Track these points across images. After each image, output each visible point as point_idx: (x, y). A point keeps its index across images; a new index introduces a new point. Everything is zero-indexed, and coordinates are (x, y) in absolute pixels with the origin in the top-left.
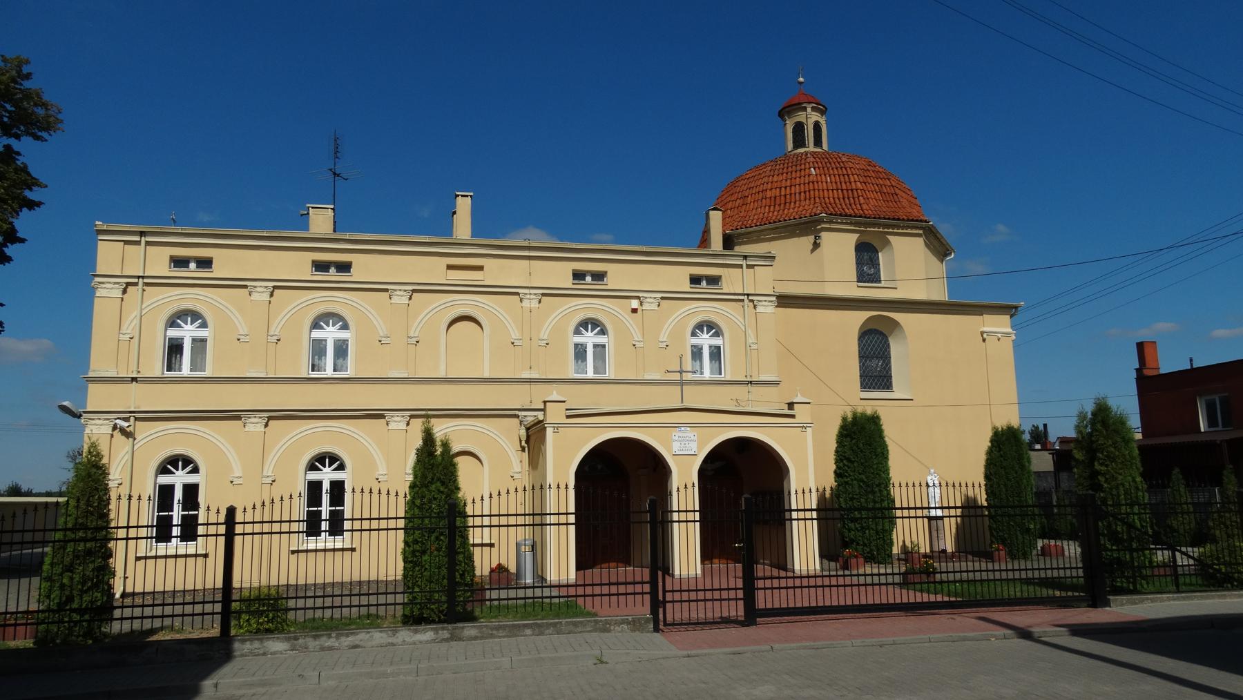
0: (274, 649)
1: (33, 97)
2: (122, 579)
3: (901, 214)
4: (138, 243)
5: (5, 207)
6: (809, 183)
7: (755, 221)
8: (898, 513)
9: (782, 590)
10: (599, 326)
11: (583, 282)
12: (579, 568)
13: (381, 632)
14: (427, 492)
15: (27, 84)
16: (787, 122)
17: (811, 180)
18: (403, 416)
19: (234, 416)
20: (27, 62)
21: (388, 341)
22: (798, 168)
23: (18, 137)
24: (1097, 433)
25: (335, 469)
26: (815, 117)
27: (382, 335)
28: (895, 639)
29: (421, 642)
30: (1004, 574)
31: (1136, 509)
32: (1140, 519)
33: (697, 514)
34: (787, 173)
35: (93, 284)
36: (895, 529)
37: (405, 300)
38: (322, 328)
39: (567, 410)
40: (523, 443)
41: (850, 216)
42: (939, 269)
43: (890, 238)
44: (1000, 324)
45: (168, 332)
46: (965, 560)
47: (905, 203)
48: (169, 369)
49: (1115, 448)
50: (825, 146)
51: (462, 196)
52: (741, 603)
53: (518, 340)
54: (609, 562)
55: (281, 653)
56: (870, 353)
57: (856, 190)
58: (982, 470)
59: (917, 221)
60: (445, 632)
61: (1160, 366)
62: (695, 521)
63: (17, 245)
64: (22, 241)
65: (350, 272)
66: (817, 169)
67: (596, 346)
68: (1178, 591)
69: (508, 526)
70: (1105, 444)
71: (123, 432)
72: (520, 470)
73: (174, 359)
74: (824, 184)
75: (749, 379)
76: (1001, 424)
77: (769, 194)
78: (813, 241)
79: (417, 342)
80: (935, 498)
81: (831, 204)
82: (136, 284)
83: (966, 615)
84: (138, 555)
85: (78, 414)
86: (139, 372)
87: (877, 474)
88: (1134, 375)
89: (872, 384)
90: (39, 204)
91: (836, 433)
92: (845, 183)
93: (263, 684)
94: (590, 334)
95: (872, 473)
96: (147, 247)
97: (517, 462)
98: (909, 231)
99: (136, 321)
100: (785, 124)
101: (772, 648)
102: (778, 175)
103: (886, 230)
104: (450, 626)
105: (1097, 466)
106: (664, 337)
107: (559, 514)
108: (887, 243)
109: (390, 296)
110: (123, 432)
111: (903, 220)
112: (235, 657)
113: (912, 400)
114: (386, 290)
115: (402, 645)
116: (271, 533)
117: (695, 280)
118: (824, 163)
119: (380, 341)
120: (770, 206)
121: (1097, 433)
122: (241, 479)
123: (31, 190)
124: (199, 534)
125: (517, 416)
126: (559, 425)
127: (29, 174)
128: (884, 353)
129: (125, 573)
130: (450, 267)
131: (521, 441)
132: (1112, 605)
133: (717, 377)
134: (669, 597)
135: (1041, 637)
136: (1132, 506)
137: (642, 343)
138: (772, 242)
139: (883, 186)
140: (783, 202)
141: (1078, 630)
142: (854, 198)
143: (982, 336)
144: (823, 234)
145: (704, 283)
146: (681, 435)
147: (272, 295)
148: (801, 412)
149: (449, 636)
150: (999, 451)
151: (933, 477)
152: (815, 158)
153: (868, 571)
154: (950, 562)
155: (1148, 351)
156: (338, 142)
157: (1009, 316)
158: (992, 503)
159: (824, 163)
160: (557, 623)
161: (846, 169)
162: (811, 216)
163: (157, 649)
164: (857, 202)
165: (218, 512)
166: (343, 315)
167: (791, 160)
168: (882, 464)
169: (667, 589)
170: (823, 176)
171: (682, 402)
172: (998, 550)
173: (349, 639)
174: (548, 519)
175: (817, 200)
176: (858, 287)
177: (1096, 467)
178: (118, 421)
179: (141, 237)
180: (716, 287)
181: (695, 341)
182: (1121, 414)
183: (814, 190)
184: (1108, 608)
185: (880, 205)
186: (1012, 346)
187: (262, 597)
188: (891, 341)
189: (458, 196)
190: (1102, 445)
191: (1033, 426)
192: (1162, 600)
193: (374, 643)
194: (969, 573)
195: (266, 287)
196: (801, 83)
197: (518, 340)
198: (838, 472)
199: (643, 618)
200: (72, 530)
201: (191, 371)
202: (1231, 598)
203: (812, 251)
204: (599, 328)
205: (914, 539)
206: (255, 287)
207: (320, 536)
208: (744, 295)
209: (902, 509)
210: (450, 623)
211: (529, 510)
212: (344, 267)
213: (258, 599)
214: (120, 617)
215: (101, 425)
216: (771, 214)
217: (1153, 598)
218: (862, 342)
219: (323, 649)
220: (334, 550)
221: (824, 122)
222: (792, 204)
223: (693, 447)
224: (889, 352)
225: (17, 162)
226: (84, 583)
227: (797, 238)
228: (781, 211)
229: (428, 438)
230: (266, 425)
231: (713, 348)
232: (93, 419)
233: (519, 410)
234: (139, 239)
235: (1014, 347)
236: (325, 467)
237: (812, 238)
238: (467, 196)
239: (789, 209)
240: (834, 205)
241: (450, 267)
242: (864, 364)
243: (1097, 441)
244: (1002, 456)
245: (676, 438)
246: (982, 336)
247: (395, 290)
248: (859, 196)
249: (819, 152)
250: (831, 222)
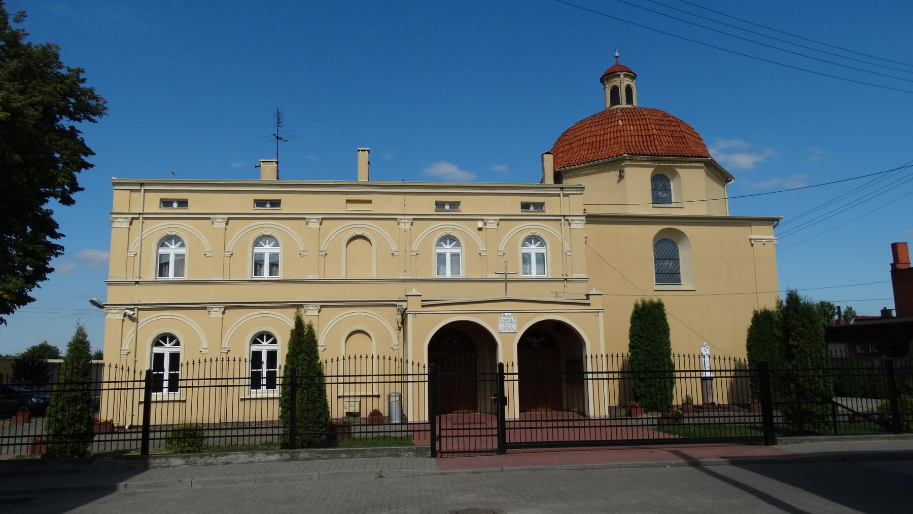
0: (174, 464)
1: (90, 93)
3: (687, 153)
4: (139, 191)
6: (617, 132)
7: (577, 161)
8: (677, 375)
9: (634, 427)
10: (539, 241)
12: (521, 411)
13: (244, 454)
14: (296, 360)
17: (618, 129)
18: (220, 308)
20: (83, 71)
21: (306, 254)
22: (610, 120)
23: (79, 120)
25: (271, 343)
26: (627, 81)
27: (301, 250)
29: (271, 461)
30: (747, 419)
34: (602, 125)
37: (317, 225)
38: (261, 246)
39: (422, 301)
40: (400, 325)
41: (647, 155)
43: (678, 170)
45: (255, 249)
47: (692, 144)
49: (804, 327)
50: (635, 103)
51: (362, 150)
53: (396, 251)
54: (463, 409)
57: (653, 135)
58: (745, 343)
59: (699, 157)
60: (287, 454)
61: (910, 261)
62: (425, 381)
63: (78, 193)
64: (82, 189)
66: (623, 121)
67: (452, 255)
68: (836, 434)
70: (796, 325)
71: (130, 317)
72: (398, 344)
73: (164, 268)
74: (629, 132)
75: (565, 277)
76: (760, 308)
78: (619, 174)
82: (138, 218)
83: (666, 449)
84: (339, 395)
85: (102, 306)
86: (140, 277)
87: (660, 346)
88: (890, 269)
90: (92, 166)
92: (645, 130)
95: (656, 346)
97: (395, 336)
98: (693, 165)
99: (139, 244)
100: (605, 88)
102: (595, 127)
103: (675, 164)
104: (290, 451)
105: (791, 342)
106: (502, 248)
107: (378, 375)
108: (676, 174)
109: (398, 223)
110: (130, 317)
111: (688, 156)
113: (695, 291)
115: (258, 463)
116: (228, 386)
117: (525, 206)
119: (300, 254)
120: (588, 150)
122: (207, 350)
130: (348, 201)
131: (398, 323)
132: (778, 443)
133: (542, 276)
134: (443, 433)
136: (816, 370)
138: (590, 176)
139: (674, 132)
141: (735, 462)
142: (651, 142)
143: (751, 242)
144: (627, 170)
145: (532, 208)
146: (505, 318)
148: (595, 303)
149: (290, 457)
150: (757, 329)
151: (705, 348)
153: (645, 416)
154: (716, 412)
155: (900, 249)
156: (280, 115)
160: (364, 450)
161: (645, 120)
162: (617, 156)
163: (100, 462)
164: (653, 144)
165: (141, 373)
167: (605, 115)
170: (628, 126)
171: (506, 295)
173: (223, 458)
174: (410, 378)
175: (623, 144)
176: (653, 207)
182: (808, 302)
183: (621, 136)
185: (671, 145)
189: (359, 150)
191: (848, 307)
192: (819, 441)
193: (240, 461)
194: (720, 418)
195: (223, 218)
196: (617, 57)
197: (396, 251)
202: (876, 440)
203: (619, 182)
204: (455, 242)
206: (216, 218)
207: (177, 391)
209: (680, 371)
210: (291, 449)
211: (249, 376)
212: (276, 204)
213: (184, 430)
218: (657, 248)
219: (206, 464)
220: (268, 399)
222: (605, 147)
223: (514, 327)
225: (78, 137)
227: (608, 173)
228: (596, 153)
229: (299, 322)
230: (224, 313)
232: (111, 310)
233: (397, 301)
234: (140, 188)
238: (365, 150)
239: (602, 151)
240: (635, 147)
241: (348, 201)
242: (658, 265)
244: (759, 333)
245: (501, 321)
246: (751, 242)
247: (310, 219)
248: (654, 140)
249: (630, 109)
250: (632, 160)
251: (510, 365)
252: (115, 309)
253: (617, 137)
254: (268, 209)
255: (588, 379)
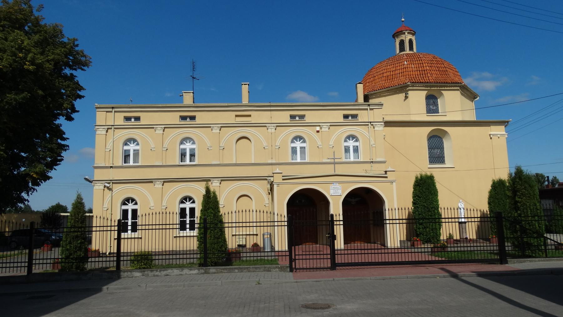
2: (109, 247)
4: (111, 112)
5: (69, 99)
7: (378, 88)
8: (443, 220)
10: (302, 139)
11: (295, 120)
12: (345, 244)
13: (177, 270)
15: (77, 49)
16: (396, 40)
19: (150, 181)
20: (77, 40)
21: (211, 148)
22: (399, 62)
23: (76, 70)
24: (517, 183)
26: (409, 37)
28: (391, 277)
31: (536, 218)
32: (539, 224)
33: (286, 223)
34: (394, 65)
35: (95, 129)
36: (442, 228)
40: (269, 191)
41: (422, 83)
42: (470, 104)
44: (500, 130)
45: (124, 147)
46: (476, 242)
47: (451, 75)
48: (125, 163)
49: (525, 190)
50: (415, 50)
51: (244, 84)
52: (329, 260)
55: (138, 277)
56: (433, 146)
57: (426, 70)
59: (456, 83)
60: (202, 270)
62: (285, 226)
64: (78, 111)
65: (195, 120)
66: (408, 62)
67: (301, 148)
69: (243, 227)
70: (521, 188)
71: (108, 188)
72: (268, 203)
73: (127, 158)
74: (411, 68)
76: (496, 178)
77: (385, 75)
78: (405, 95)
79: (224, 149)
80: (463, 213)
81: (413, 78)
82: (111, 128)
84: (115, 238)
86: (113, 164)
89: (434, 161)
90: (83, 97)
91: (413, 184)
92: (421, 67)
93: (125, 288)
94: (351, 142)
96: (115, 113)
97: (266, 198)
98: (452, 88)
99: (112, 144)
100: (395, 41)
101: (334, 279)
103: (441, 88)
105: (517, 199)
106: (331, 143)
107: (257, 222)
110: (108, 188)
111: (449, 83)
112: (121, 278)
114: (210, 127)
115: (185, 275)
117: (346, 117)
118: (411, 59)
120: (385, 80)
121: (517, 183)
122: (154, 207)
123: (80, 91)
124: (129, 229)
125: (267, 180)
126: (279, 183)
127: (79, 85)
128: (440, 146)
129: (110, 245)
130: (237, 116)
131: (268, 190)
132: (509, 263)
133: (357, 160)
134: (297, 257)
135: (462, 277)
136: (534, 217)
137: (322, 146)
138: (386, 97)
140: (391, 78)
141: (481, 275)
142: (425, 74)
143: (490, 136)
144: (410, 92)
145: (350, 118)
147: (164, 131)
152: (407, 56)
157: (504, 126)
158: (491, 215)
159: (411, 59)
160: (249, 267)
161: (422, 61)
162: (404, 84)
165: (115, 221)
166: (193, 138)
167: (396, 58)
168: (434, 198)
169: (296, 254)
171: (335, 172)
172: (492, 238)
173: (164, 272)
174: (276, 224)
177: (516, 199)
178: (106, 184)
179: (112, 109)
180: (356, 119)
181: (346, 144)
184: (507, 265)
186: (506, 142)
187: (146, 254)
188: (444, 140)
189: (242, 84)
190: (519, 188)
191: (553, 177)
193: (174, 274)
195: (161, 128)
196: (403, 21)
198: (414, 202)
199: (285, 266)
200: (71, 228)
201: (133, 163)
203: (405, 100)
204: (355, 139)
205: (451, 232)
206: (157, 128)
208: (369, 122)
209: (445, 218)
212: (193, 118)
214: (7, 264)
215: (100, 186)
216: (386, 84)
217: (531, 260)
219: (154, 276)
221: (415, 39)
223: (340, 192)
224: (443, 146)
226: (76, 248)
229: (208, 190)
230: (163, 185)
231: (355, 147)
232: (97, 183)
234: (112, 110)
235: (507, 142)
236: (187, 202)
237: (404, 94)
238: (246, 84)
239: (394, 81)
240: (415, 78)
241: (237, 116)
242: (430, 152)
243: (517, 187)
244: (496, 193)
245: (332, 188)
246: (490, 136)
247: (214, 127)
249: (411, 54)
250: (413, 86)
251: (338, 215)
252: (99, 183)
253: (404, 72)
254: (188, 121)
255: (386, 224)
